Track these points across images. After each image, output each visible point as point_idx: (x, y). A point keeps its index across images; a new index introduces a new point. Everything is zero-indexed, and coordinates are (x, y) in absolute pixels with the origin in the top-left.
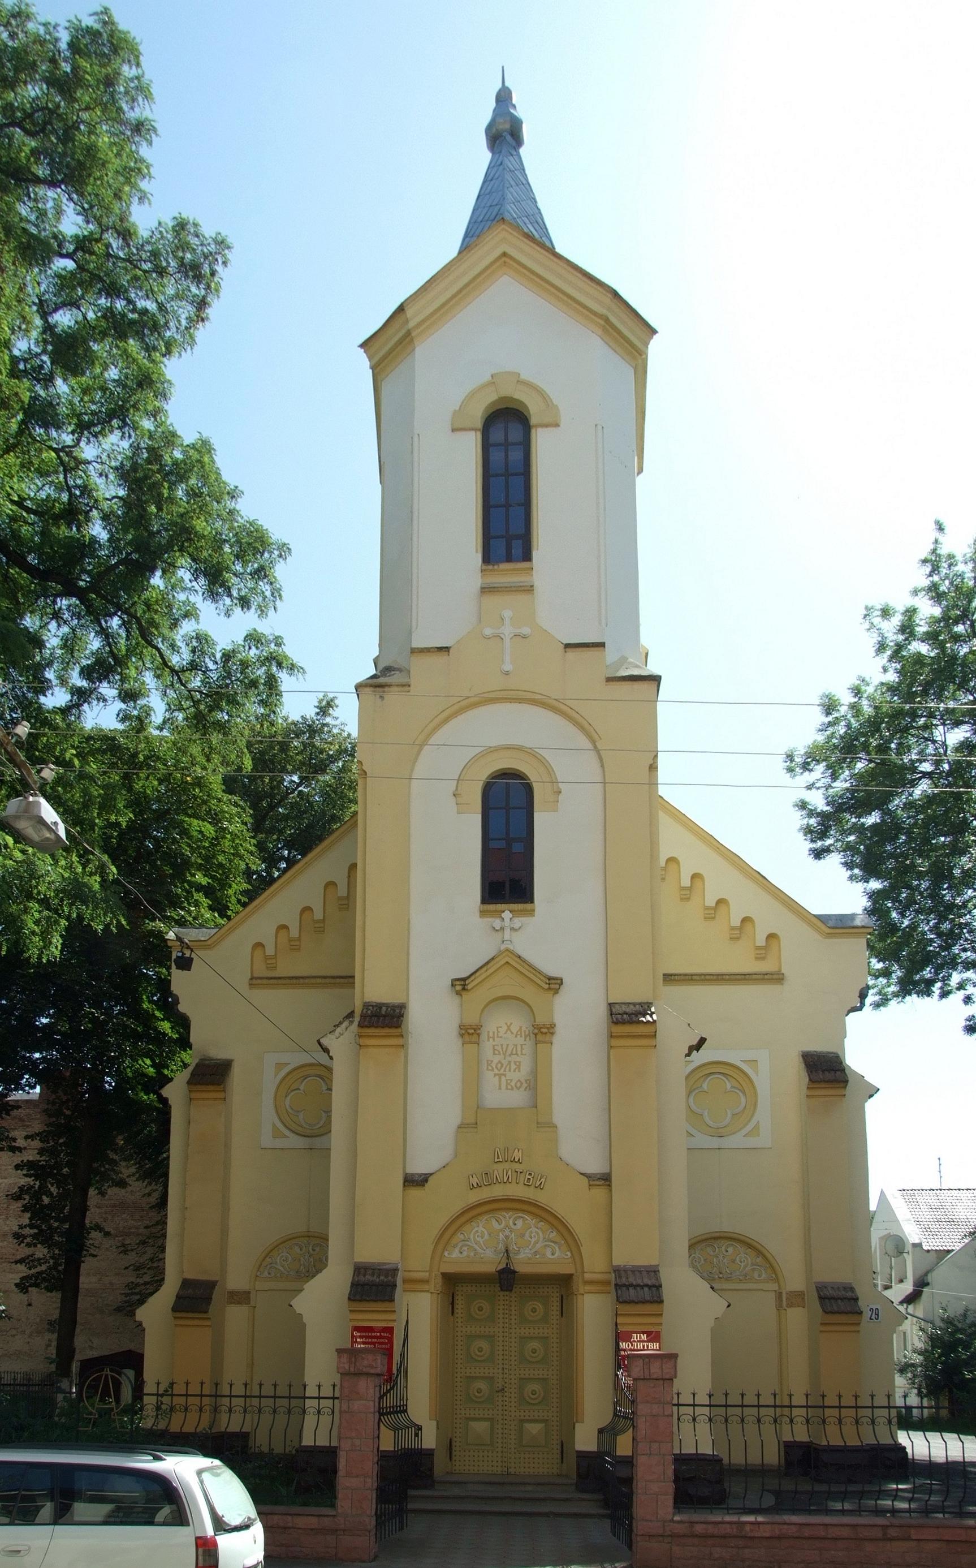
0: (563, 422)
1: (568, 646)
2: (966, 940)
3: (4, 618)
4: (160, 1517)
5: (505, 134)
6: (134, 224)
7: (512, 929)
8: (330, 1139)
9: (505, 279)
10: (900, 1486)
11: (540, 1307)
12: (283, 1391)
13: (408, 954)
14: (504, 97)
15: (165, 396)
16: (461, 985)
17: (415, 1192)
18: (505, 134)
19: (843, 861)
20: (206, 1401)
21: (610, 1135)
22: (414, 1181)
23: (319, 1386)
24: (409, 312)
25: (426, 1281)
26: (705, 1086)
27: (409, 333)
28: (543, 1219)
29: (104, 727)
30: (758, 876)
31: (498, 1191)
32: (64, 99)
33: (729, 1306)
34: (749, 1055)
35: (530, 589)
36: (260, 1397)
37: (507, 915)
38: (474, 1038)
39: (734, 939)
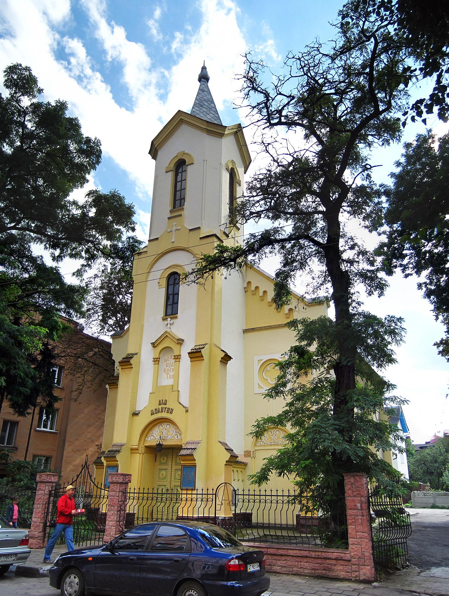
0: (195, 162)
1: (190, 230)
2: (439, 280)
3: (1, 313)
4: (196, 101)
5: (204, 78)
6: (126, 83)
7: (170, 324)
8: (110, 159)
9: (183, 125)
10: (56, 377)
11: (165, 459)
12: (274, 493)
13: (424, 508)
14: (204, 68)
15: (9, 22)
16: (154, 345)
17: (136, 418)
18: (204, 78)
19: (79, 187)
20: (141, 495)
21: (158, 375)
22: (135, 414)
23: (208, 489)
24: (155, 143)
25: (137, 449)
26: (268, 369)
27: (156, 148)
28: (165, 422)
29: (245, 42)
30: (175, 538)
31: (159, 415)
32: (334, 410)
33: (187, 411)
34: (256, 362)
35: (202, 356)
36: (271, 496)
37: (169, 319)
38: (178, 360)
39: (262, 300)
